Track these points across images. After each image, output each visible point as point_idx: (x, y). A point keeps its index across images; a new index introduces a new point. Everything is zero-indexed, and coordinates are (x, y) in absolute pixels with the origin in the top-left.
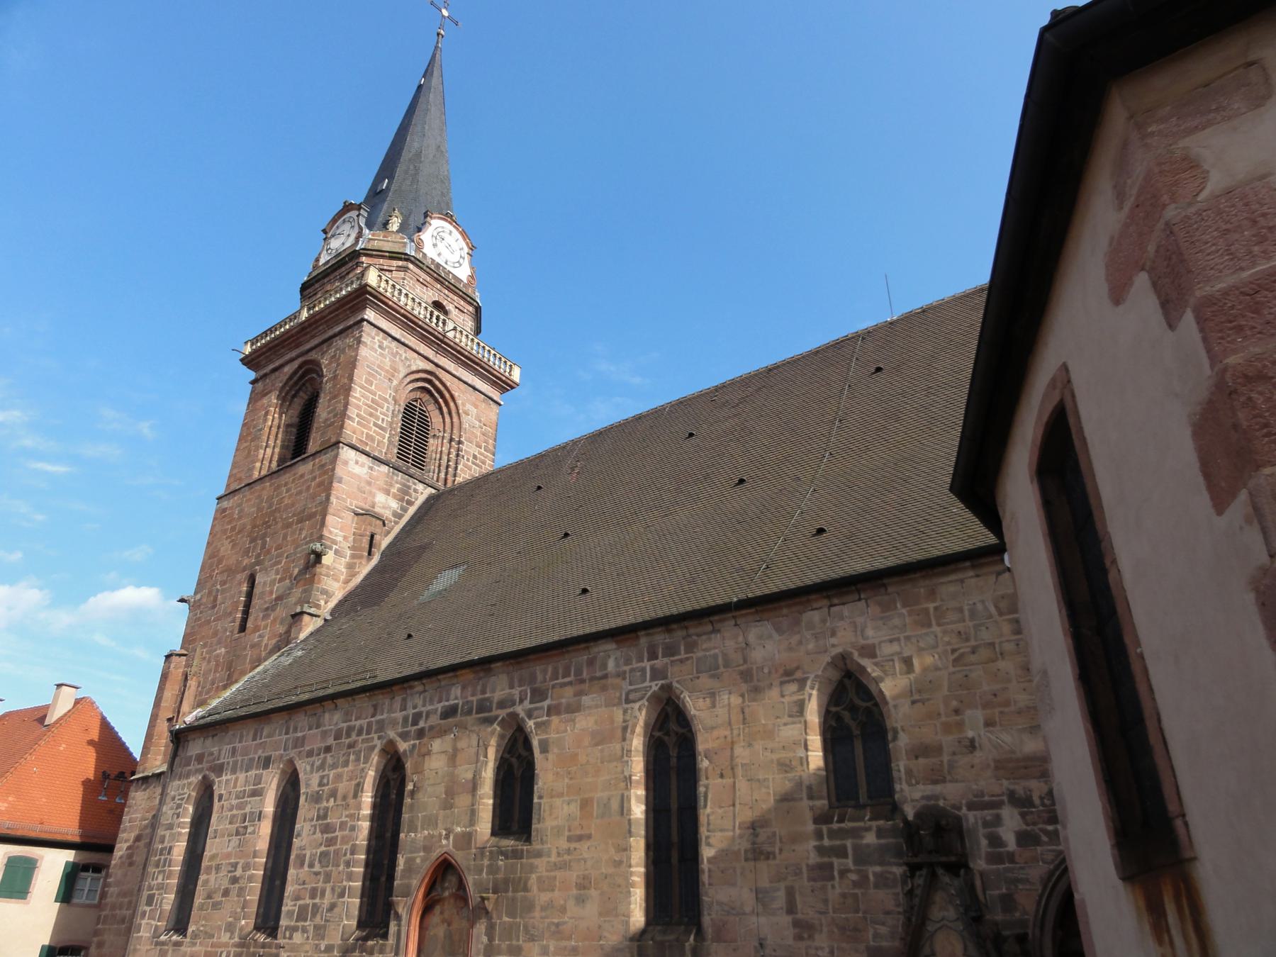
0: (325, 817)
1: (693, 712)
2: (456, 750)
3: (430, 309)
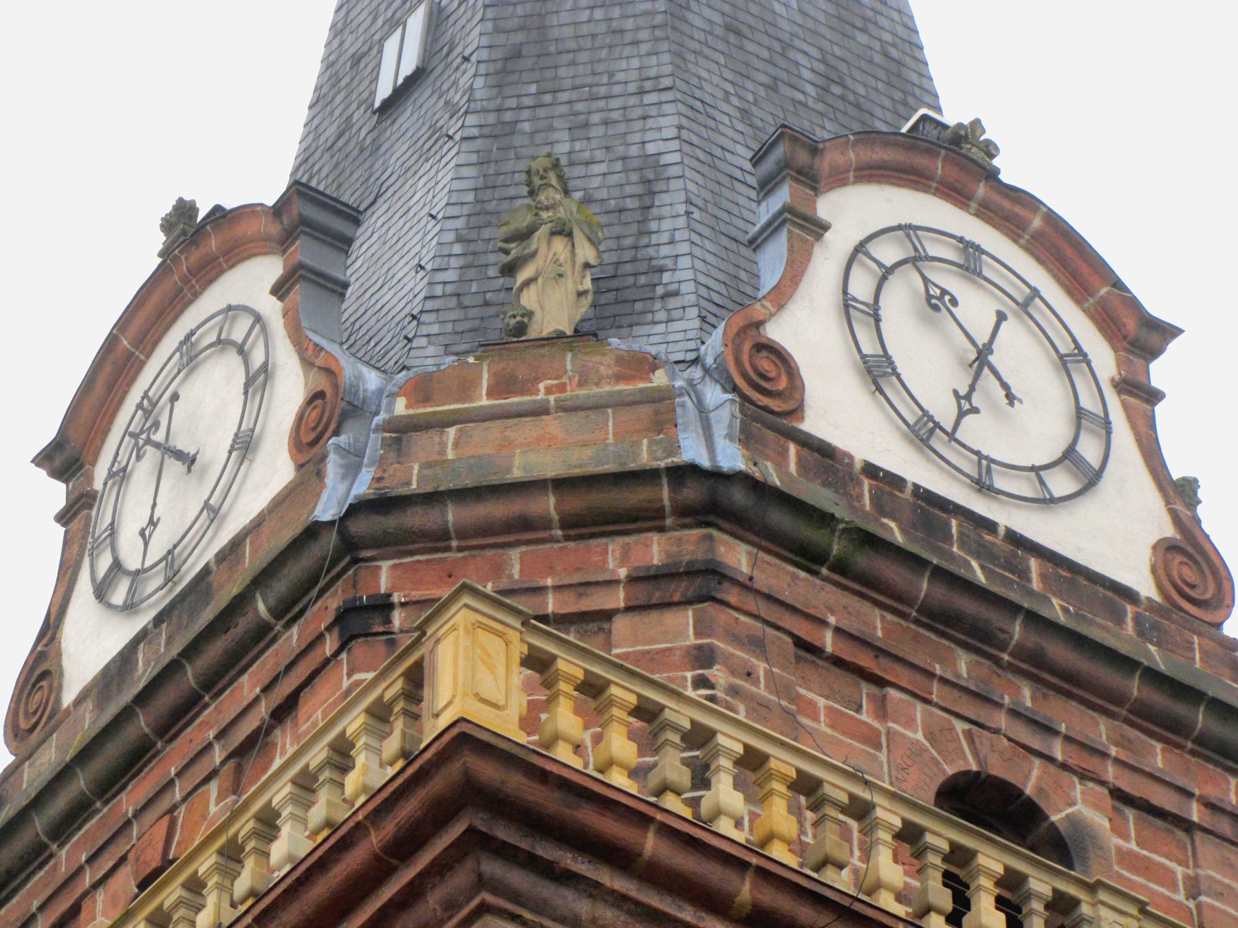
3: (942, 835)
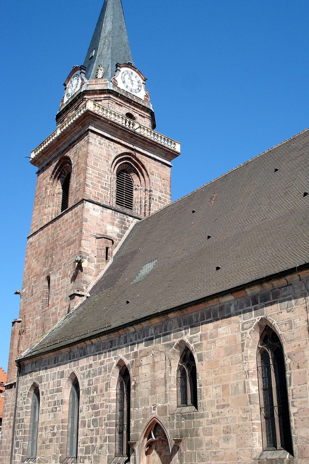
0: (93, 401)
1: (280, 332)
2: (154, 363)
